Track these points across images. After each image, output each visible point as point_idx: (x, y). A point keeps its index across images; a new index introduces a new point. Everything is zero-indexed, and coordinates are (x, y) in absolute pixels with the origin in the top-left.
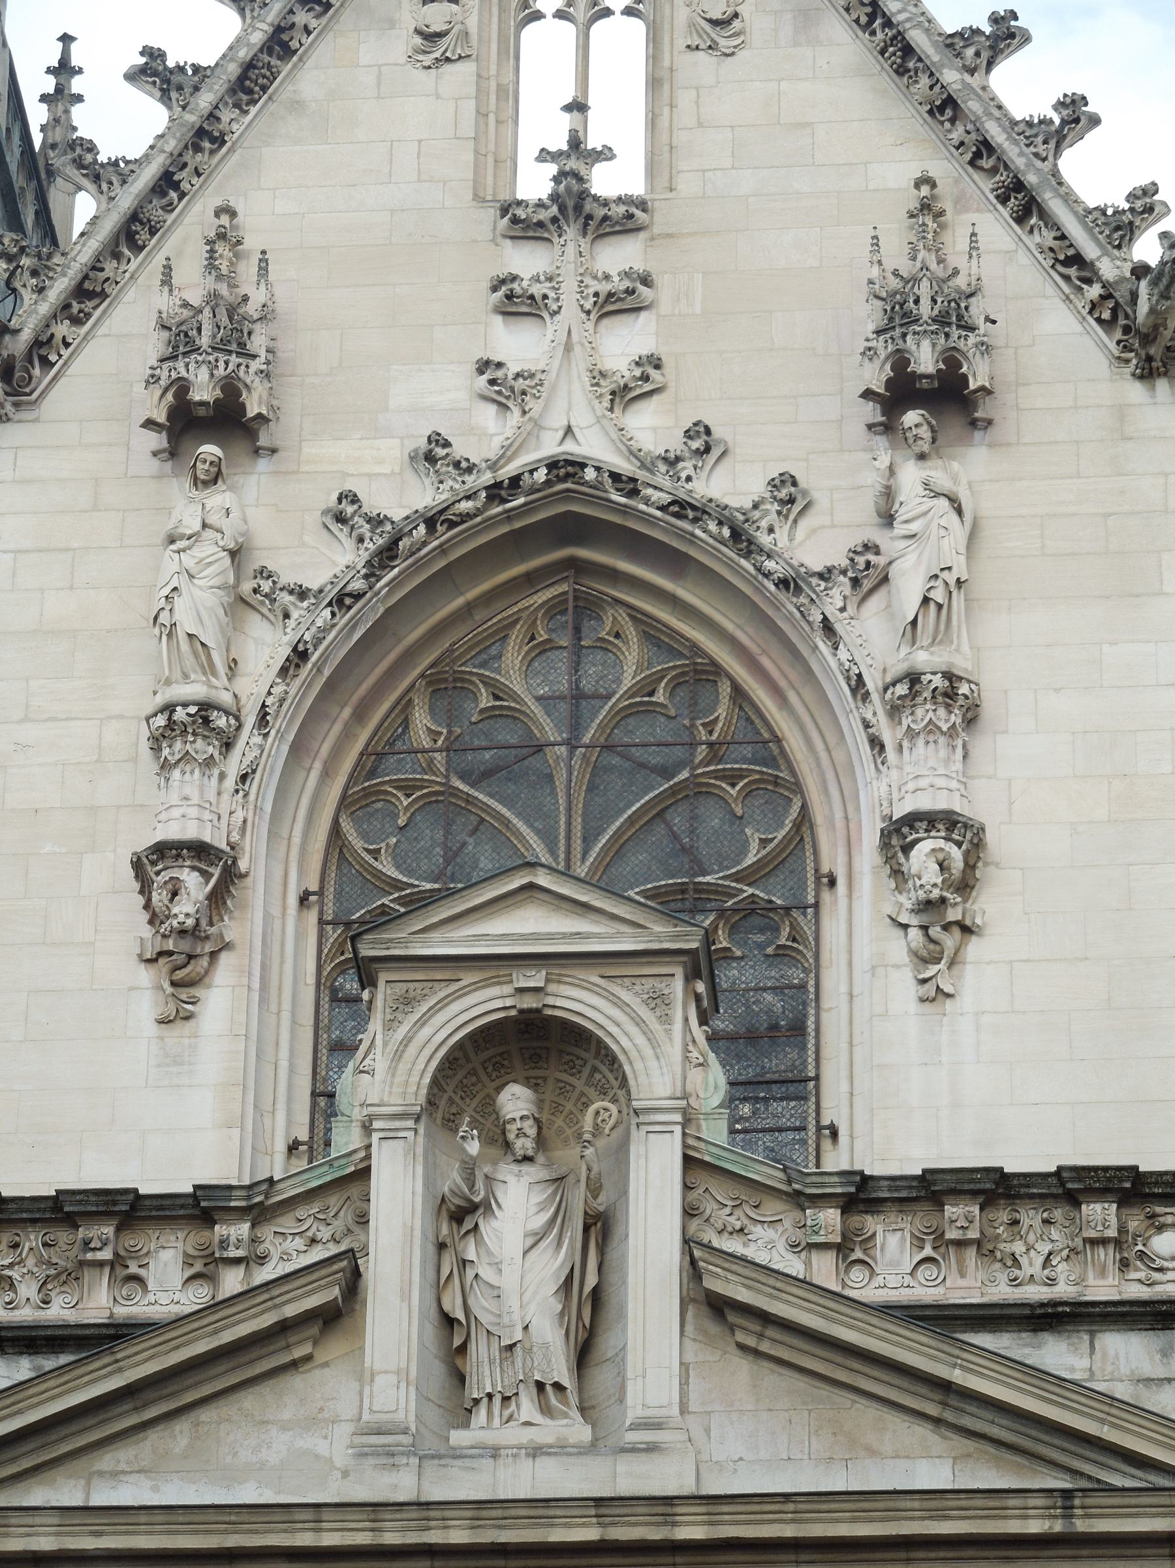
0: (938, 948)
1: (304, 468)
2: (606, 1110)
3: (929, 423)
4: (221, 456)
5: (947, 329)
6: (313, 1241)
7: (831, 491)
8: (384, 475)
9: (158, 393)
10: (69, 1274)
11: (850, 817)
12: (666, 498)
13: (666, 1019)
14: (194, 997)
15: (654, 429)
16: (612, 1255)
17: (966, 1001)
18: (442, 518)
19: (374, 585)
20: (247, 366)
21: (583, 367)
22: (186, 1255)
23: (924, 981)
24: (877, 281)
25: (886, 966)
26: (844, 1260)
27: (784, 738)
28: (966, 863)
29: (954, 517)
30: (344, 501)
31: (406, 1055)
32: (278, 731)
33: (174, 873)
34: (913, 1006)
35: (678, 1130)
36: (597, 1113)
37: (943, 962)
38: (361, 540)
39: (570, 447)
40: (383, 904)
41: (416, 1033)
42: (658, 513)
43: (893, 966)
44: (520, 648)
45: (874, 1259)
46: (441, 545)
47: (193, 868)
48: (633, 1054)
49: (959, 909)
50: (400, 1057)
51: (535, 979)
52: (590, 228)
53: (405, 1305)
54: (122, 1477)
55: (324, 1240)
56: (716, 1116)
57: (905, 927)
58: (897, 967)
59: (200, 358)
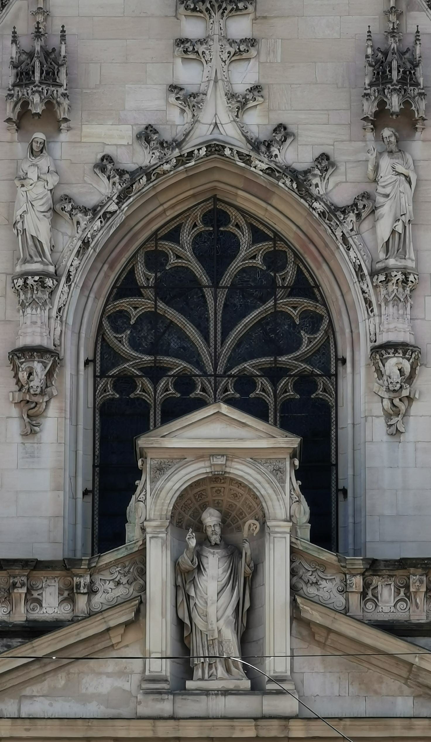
0: (397, 409)
1: (84, 140)
2: (254, 524)
3: (395, 135)
4: (45, 139)
5: (405, 87)
6: (118, 583)
7: (346, 162)
8: (124, 145)
9: (12, 105)
10: (6, 598)
11: (353, 331)
12: (264, 166)
13: (282, 481)
14: (39, 423)
15: (258, 125)
16: (258, 591)
17: (410, 436)
18: (154, 172)
19: (121, 207)
20: (57, 91)
21: (223, 93)
22: (59, 589)
23: (391, 425)
24: (370, 56)
25: (372, 416)
26: (363, 600)
27: (320, 286)
28: (412, 367)
29: (407, 185)
30: (105, 160)
31: (161, 495)
32: (75, 283)
33: (30, 364)
34: (385, 438)
35: (288, 536)
36: (250, 525)
37: (400, 416)
38: (114, 184)
39: (216, 135)
40: (125, 367)
41: (165, 485)
42: (261, 173)
43: (376, 416)
44: (189, 233)
45: (377, 599)
46: (154, 185)
47: (39, 362)
48: (267, 498)
49: (408, 390)
50: (158, 497)
51: (221, 461)
52: (225, 14)
53: (164, 620)
54: (35, 699)
55: (124, 583)
56: (304, 527)
57: (382, 398)
58: (377, 417)
59: (34, 89)
